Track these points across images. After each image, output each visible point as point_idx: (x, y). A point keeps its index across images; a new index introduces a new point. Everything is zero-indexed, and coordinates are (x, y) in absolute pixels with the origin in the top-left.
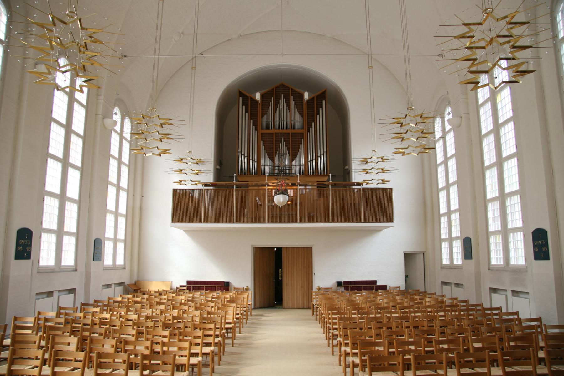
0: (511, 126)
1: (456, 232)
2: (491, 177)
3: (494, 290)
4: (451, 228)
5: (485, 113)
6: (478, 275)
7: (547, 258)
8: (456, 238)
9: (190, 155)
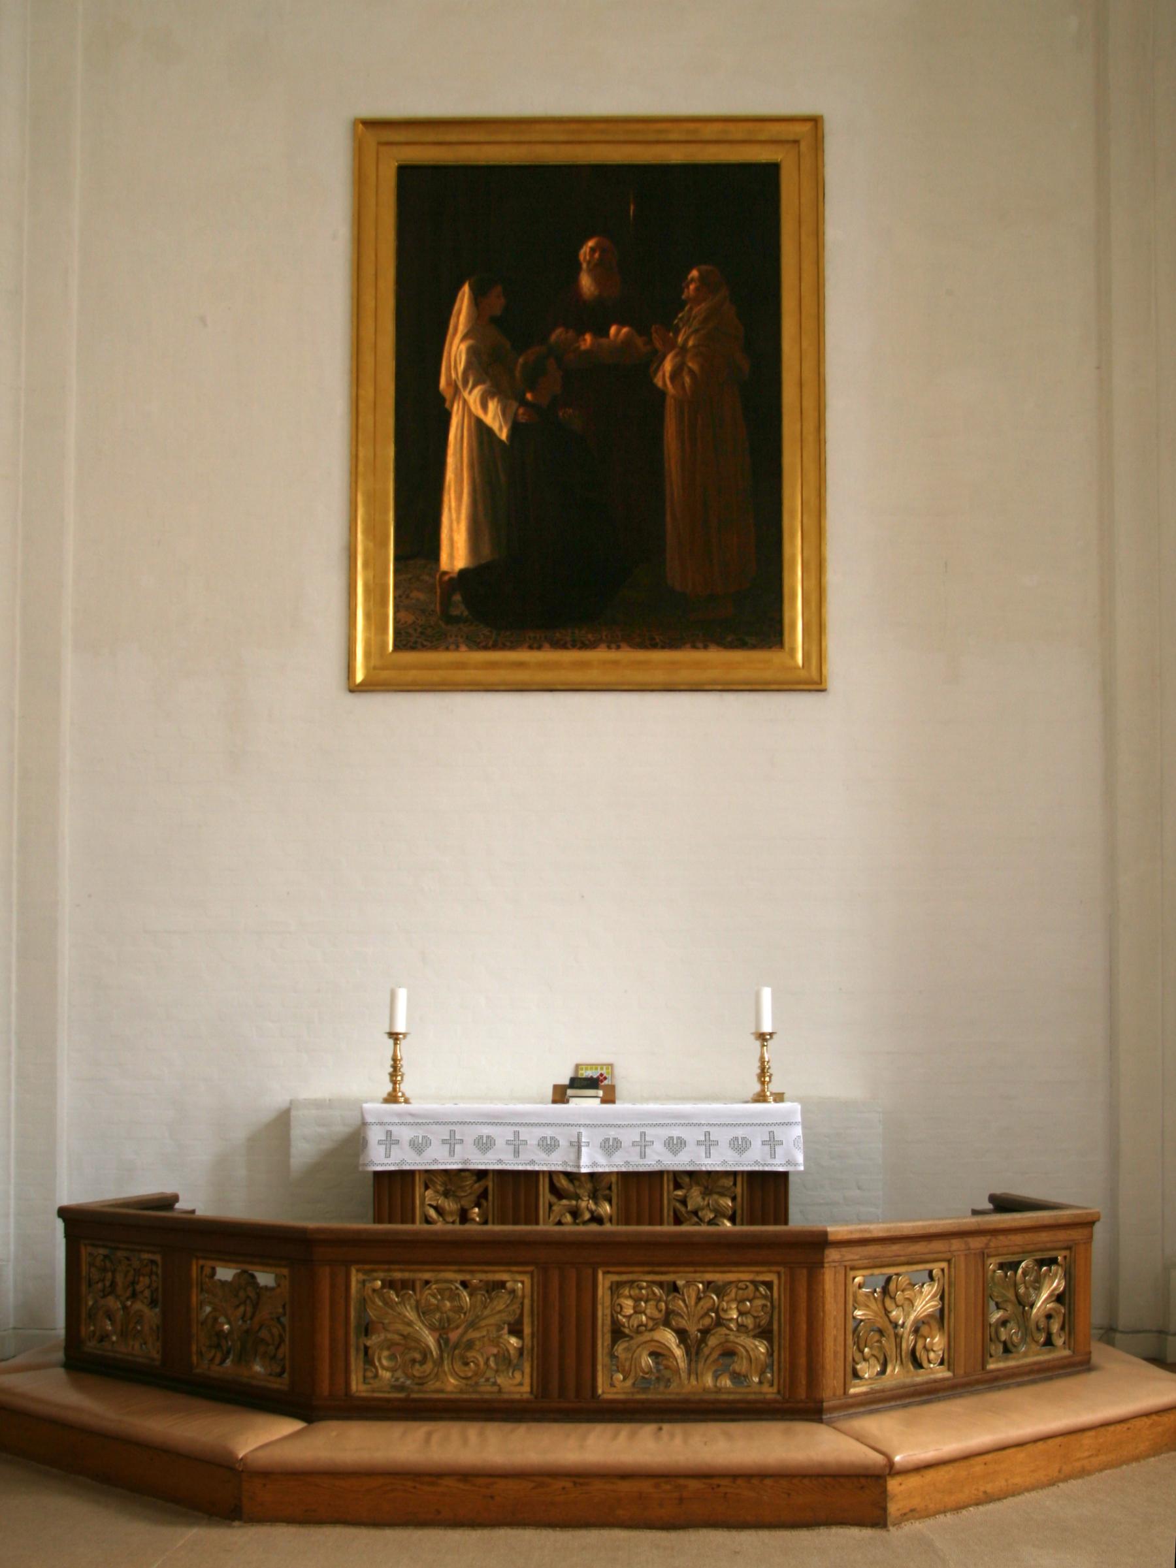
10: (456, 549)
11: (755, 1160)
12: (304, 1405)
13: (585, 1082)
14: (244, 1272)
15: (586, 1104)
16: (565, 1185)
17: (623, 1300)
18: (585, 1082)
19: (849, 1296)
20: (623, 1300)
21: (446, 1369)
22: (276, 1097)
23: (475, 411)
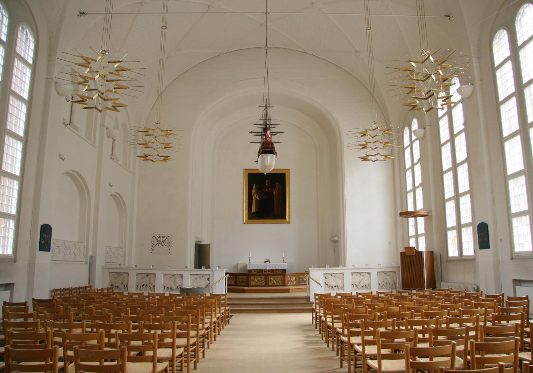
0: (463, 135)
1: (466, 217)
2: (448, 178)
3: (518, 282)
4: (461, 213)
5: (444, 124)
6: (497, 265)
7: (488, 247)
8: (467, 225)
9: (158, 126)
10: (254, 210)
11: (283, 268)
12: (248, 286)
13: (267, 261)
14: (27, 320)
15: (267, 263)
16: (265, 271)
17: (271, 278)
18: (267, 261)
19: (288, 278)
20: (271, 278)
21: (456, 97)
22: (236, 263)
23: (256, 197)
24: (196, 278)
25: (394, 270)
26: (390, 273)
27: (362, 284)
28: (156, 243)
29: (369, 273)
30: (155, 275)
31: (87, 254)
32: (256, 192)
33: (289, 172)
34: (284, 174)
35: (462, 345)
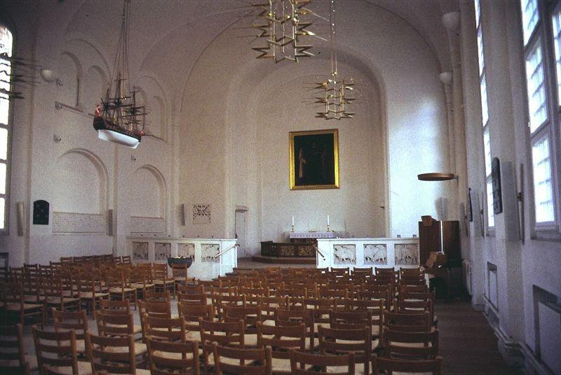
7: (46, 222)
10: (301, 175)
12: (277, 256)
24: (207, 248)
25: (416, 242)
26: (410, 246)
27: (376, 258)
28: (197, 212)
29: (385, 245)
30: (170, 244)
31: (517, 191)
32: (303, 156)
33: (338, 132)
34: (295, 137)
35: (344, 365)
